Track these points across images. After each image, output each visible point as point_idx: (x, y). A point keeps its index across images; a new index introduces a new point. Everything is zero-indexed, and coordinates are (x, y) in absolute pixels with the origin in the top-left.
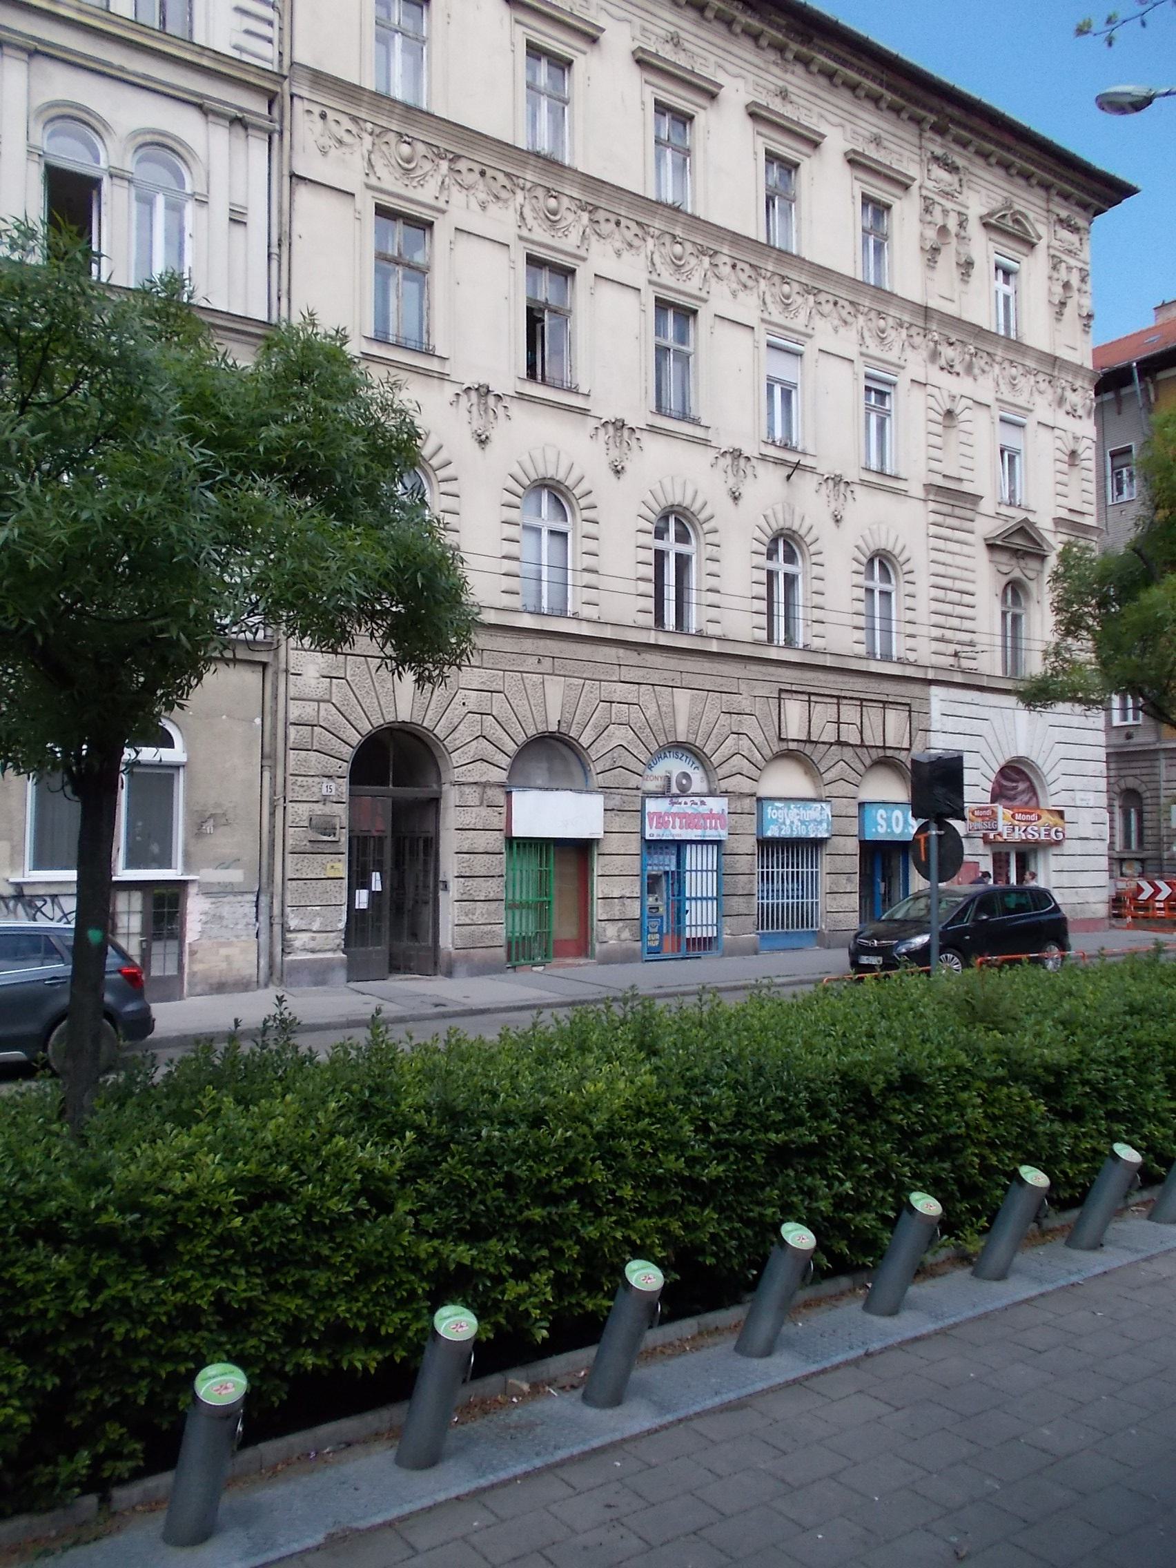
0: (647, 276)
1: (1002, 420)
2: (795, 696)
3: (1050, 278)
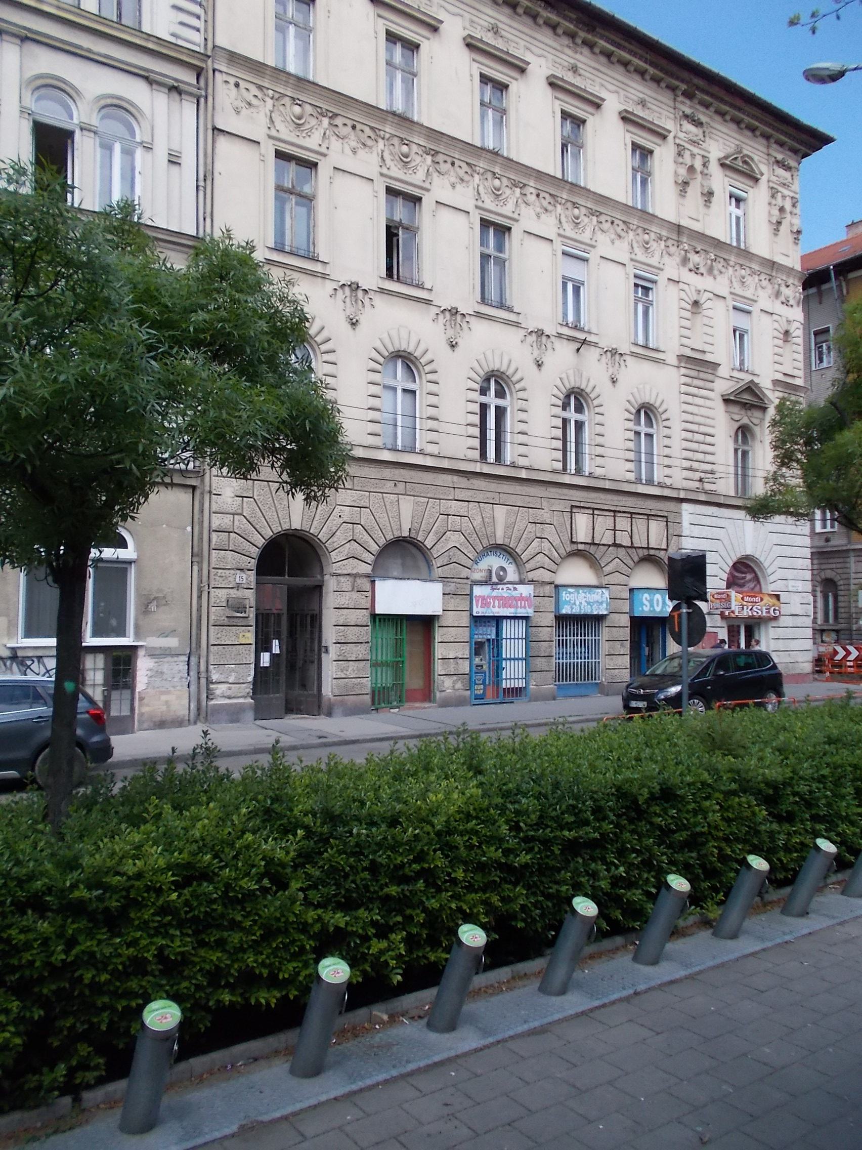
0: (474, 202)
1: (735, 308)
2: (583, 510)
3: (770, 204)
